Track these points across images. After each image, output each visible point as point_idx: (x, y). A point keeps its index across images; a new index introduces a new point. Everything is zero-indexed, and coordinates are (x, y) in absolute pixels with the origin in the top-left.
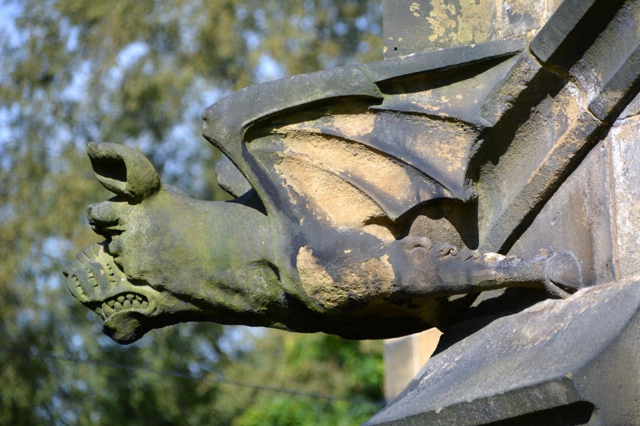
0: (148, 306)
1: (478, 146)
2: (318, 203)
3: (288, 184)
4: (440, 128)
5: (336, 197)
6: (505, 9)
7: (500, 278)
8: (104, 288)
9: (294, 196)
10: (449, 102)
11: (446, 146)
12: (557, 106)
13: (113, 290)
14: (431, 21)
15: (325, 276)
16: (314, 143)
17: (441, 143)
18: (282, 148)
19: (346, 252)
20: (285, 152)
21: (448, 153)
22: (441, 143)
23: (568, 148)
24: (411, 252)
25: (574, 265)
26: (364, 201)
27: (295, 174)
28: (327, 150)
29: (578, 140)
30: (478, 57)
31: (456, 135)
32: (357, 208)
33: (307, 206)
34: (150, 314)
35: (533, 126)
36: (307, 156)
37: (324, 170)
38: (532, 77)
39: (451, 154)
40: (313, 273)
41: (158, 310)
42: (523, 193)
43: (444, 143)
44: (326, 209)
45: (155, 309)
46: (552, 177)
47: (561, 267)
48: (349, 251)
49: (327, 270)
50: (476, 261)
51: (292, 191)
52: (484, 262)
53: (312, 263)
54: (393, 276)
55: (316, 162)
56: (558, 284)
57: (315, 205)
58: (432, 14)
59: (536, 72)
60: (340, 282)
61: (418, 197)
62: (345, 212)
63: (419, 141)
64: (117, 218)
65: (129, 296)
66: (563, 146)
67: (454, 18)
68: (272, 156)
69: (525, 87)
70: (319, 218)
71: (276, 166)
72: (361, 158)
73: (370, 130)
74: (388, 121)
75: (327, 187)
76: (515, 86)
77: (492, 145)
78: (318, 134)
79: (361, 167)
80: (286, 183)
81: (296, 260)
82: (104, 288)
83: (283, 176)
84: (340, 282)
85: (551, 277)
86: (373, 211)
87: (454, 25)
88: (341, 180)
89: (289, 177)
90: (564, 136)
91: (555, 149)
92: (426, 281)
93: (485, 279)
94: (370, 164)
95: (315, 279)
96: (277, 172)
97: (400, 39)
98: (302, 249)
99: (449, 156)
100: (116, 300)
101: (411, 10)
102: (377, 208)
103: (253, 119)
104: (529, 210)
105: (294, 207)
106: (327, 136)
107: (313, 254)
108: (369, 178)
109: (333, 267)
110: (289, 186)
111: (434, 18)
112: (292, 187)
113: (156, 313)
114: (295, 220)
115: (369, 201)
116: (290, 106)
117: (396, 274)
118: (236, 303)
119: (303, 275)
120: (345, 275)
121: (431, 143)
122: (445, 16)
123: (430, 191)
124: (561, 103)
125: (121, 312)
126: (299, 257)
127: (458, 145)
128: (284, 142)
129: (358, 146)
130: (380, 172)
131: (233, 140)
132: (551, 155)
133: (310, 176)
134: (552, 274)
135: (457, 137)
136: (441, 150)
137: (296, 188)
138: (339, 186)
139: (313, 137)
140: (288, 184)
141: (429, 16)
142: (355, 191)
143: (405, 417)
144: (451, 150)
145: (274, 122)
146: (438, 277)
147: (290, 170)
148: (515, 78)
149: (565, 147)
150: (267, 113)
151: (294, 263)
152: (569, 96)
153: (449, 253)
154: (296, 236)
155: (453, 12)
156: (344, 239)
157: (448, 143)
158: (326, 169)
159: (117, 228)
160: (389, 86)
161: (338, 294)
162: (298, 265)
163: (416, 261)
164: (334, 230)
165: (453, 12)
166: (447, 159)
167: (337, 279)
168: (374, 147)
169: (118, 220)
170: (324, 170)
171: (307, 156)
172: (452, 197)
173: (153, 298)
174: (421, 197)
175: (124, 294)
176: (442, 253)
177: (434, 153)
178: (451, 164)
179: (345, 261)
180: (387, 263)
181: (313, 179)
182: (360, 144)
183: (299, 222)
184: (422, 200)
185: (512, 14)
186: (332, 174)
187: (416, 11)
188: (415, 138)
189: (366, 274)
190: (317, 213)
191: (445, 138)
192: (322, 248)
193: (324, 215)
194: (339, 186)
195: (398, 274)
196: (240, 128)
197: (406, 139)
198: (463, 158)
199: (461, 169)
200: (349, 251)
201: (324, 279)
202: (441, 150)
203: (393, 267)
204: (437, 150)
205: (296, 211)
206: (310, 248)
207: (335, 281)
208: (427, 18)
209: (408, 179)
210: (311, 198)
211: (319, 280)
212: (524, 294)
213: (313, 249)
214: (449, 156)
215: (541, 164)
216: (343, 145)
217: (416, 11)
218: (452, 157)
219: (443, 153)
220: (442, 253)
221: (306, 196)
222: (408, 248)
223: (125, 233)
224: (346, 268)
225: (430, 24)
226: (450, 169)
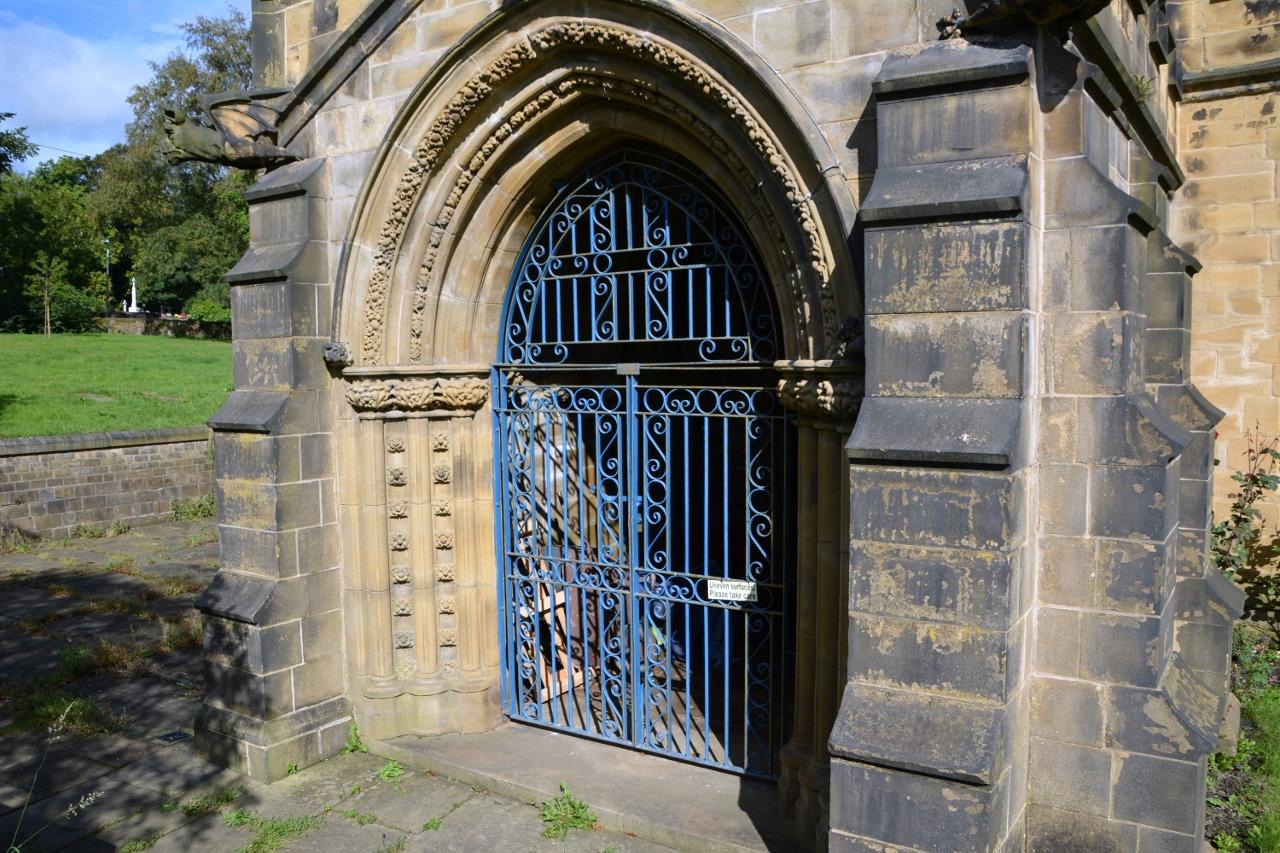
39: (271, 119)
62: (239, 133)
77: (283, 117)
130: (250, 122)
156: (239, 140)
160: (253, 98)
168: (249, 115)
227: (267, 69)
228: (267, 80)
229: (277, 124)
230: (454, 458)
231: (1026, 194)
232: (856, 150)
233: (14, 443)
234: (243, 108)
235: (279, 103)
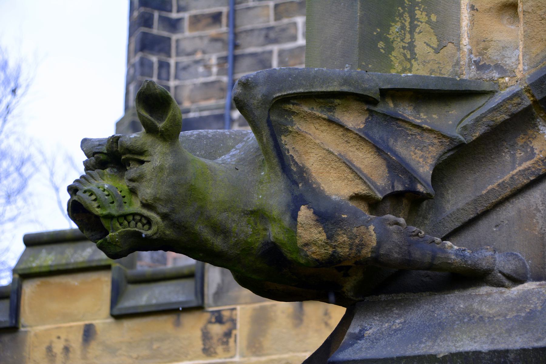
0: (149, 229)
1: (445, 157)
2: (314, 174)
3: (290, 154)
4: (418, 137)
5: (328, 172)
6: (471, 60)
7: (457, 263)
8: (120, 206)
9: (294, 164)
10: (427, 118)
11: (419, 152)
12: (523, 138)
13: (127, 209)
14: (393, 58)
15: (320, 233)
16: (317, 126)
17: (416, 149)
18: (292, 123)
19: (343, 216)
20: (294, 127)
21: (420, 158)
22: (416, 149)
23: (533, 172)
24: (391, 227)
25: (524, 263)
26: (353, 180)
27: (297, 148)
28: (325, 134)
29: (543, 167)
30: (472, 89)
31: (430, 145)
32: (345, 184)
33: (305, 175)
34: (150, 236)
35: (493, 151)
36: (310, 134)
37: (324, 149)
38: (519, 110)
39: (422, 161)
40: (311, 228)
41: (158, 235)
42: (475, 201)
43: (418, 150)
44: (319, 180)
45: (155, 233)
46: (508, 192)
47: (513, 262)
48: (346, 216)
49: (324, 228)
50: (438, 246)
51: (294, 160)
52: (445, 248)
53: (313, 220)
54: (374, 244)
55: (317, 141)
56: (504, 274)
57: (310, 175)
58: (393, 53)
59: (525, 107)
60: (331, 240)
61: (393, 187)
62: (338, 187)
63: (399, 143)
64: (146, 149)
65: (138, 218)
66: (529, 168)
67: (409, 60)
68: (283, 128)
69: (507, 117)
70: (314, 186)
71: (283, 137)
72: (351, 146)
73: (362, 126)
74: (376, 122)
75: (322, 163)
76: (501, 115)
77: (459, 157)
78: (324, 119)
79: (351, 154)
80: (288, 152)
81: (297, 215)
82: (120, 206)
83: (287, 147)
84: (331, 240)
85: (501, 269)
86: (361, 189)
87: (408, 66)
88: (337, 160)
89: (291, 148)
90: (531, 162)
91: (520, 171)
92: (399, 253)
93: (445, 260)
94: (357, 153)
95: (311, 233)
96: (283, 142)
97: (370, 66)
98: (303, 207)
99: (421, 160)
100: (125, 219)
101: (379, 46)
102: (364, 187)
103: (283, 94)
104: (476, 215)
105: (295, 173)
106: (331, 121)
107: (314, 213)
108: (357, 164)
109: (330, 226)
110: (291, 155)
111: (394, 57)
112: (293, 157)
113: (155, 237)
114: (296, 183)
115: (359, 181)
116: (313, 90)
117: (378, 243)
118: (218, 243)
119: (301, 228)
120: (338, 235)
121: (408, 147)
122: (403, 58)
123: (403, 184)
124: (527, 137)
125: (126, 229)
126: (300, 213)
127: (429, 153)
128: (294, 120)
129: (354, 136)
130: (365, 159)
131: (264, 106)
132: (514, 175)
133: (309, 151)
134: (503, 267)
135: (430, 147)
136: (415, 154)
137: (297, 160)
138: (333, 164)
139: (318, 121)
140: (290, 154)
141: (391, 55)
142: (348, 170)
143: (395, 357)
144: (422, 156)
145: (292, 101)
146: (409, 253)
147: (294, 143)
148: (503, 109)
149: (530, 171)
150: (295, 91)
151: (294, 217)
152: (537, 132)
153: (417, 235)
154: (296, 196)
155: (409, 57)
156: (338, 207)
157: (421, 150)
158: (327, 148)
159: (142, 158)
160: (384, 93)
161: (325, 250)
162: (299, 219)
163: (395, 235)
164: (328, 198)
165: (409, 57)
166: (419, 162)
167: (330, 237)
168: (364, 138)
169: (146, 151)
170: (324, 149)
171: (310, 134)
172: (425, 192)
173: (157, 223)
174: (395, 187)
175: (134, 215)
176: (413, 234)
177: (410, 155)
178: (422, 167)
179: (341, 223)
180: (373, 233)
181: (311, 155)
182: (357, 134)
183: (298, 186)
184: (396, 190)
185: (480, 64)
186: (330, 153)
187: (382, 48)
188: (396, 140)
189: (354, 238)
190: (312, 181)
191: (421, 146)
192: (322, 210)
193: (319, 185)
194: (333, 164)
195: (379, 243)
196: (272, 99)
197: (389, 140)
198: (431, 164)
199: (429, 172)
200: (346, 216)
201: (319, 235)
202: (415, 154)
203: (377, 237)
204: (412, 153)
205: (296, 177)
206: (311, 208)
207: (328, 238)
208: (390, 56)
209: (386, 171)
210: (308, 169)
211: (313, 235)
212: (469, 277)
213: (313, 209)
214: (421, 160)
215: (501, 181)
216: (340, 132)
217: (382, 48)
218: (423, 161)
219: (416, 157)
220: (413, 234)
221: (304, 166)
222: (389, 224)
223: (148, 163)
224: (339, 229)
225: (392, 61)
226: (421, 170)
227: (395, 28)
228: (396, 56)
229: (443, 171)
230: (75, 252)
231: (395, 316)
232: (346, 309)
233: (534, 40)
234: (354, 119)
235: (453, 121)
